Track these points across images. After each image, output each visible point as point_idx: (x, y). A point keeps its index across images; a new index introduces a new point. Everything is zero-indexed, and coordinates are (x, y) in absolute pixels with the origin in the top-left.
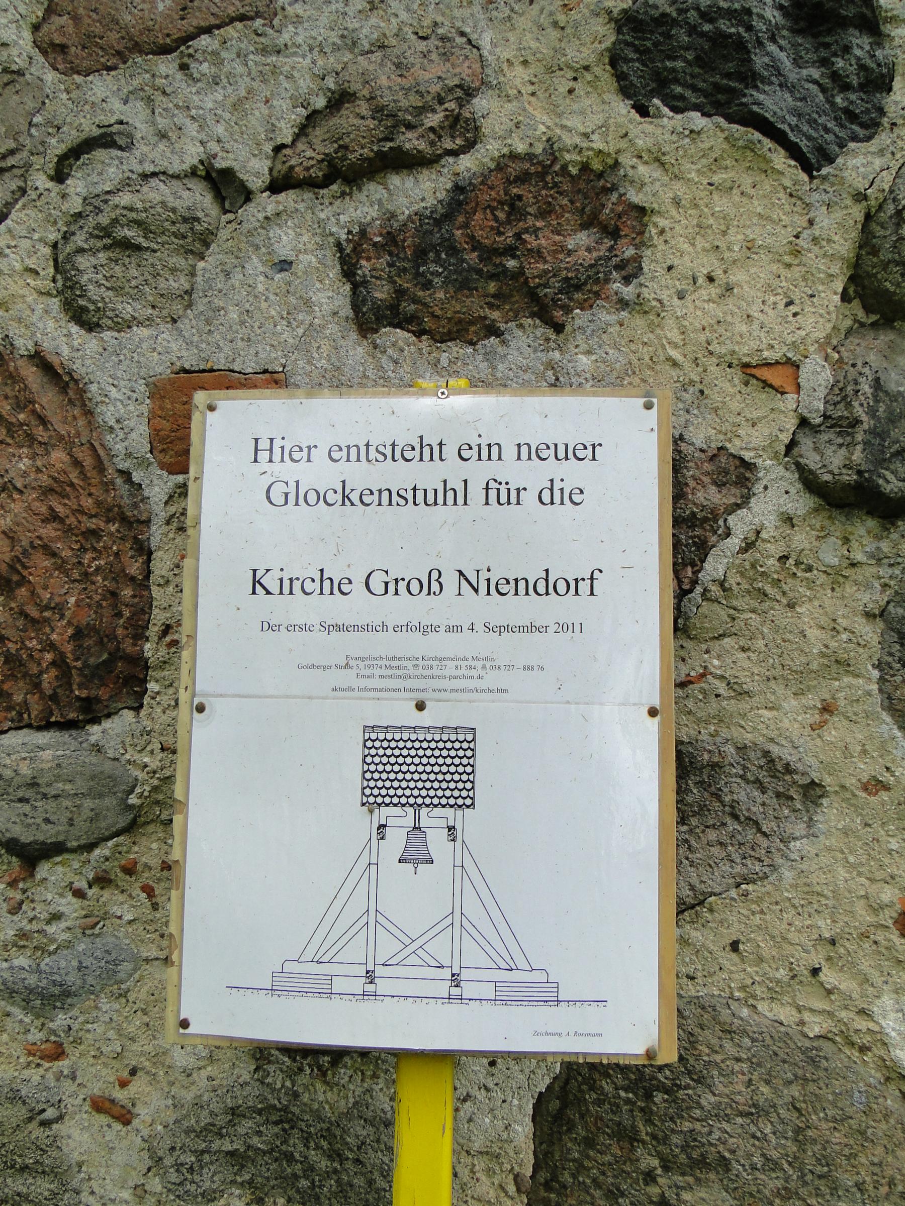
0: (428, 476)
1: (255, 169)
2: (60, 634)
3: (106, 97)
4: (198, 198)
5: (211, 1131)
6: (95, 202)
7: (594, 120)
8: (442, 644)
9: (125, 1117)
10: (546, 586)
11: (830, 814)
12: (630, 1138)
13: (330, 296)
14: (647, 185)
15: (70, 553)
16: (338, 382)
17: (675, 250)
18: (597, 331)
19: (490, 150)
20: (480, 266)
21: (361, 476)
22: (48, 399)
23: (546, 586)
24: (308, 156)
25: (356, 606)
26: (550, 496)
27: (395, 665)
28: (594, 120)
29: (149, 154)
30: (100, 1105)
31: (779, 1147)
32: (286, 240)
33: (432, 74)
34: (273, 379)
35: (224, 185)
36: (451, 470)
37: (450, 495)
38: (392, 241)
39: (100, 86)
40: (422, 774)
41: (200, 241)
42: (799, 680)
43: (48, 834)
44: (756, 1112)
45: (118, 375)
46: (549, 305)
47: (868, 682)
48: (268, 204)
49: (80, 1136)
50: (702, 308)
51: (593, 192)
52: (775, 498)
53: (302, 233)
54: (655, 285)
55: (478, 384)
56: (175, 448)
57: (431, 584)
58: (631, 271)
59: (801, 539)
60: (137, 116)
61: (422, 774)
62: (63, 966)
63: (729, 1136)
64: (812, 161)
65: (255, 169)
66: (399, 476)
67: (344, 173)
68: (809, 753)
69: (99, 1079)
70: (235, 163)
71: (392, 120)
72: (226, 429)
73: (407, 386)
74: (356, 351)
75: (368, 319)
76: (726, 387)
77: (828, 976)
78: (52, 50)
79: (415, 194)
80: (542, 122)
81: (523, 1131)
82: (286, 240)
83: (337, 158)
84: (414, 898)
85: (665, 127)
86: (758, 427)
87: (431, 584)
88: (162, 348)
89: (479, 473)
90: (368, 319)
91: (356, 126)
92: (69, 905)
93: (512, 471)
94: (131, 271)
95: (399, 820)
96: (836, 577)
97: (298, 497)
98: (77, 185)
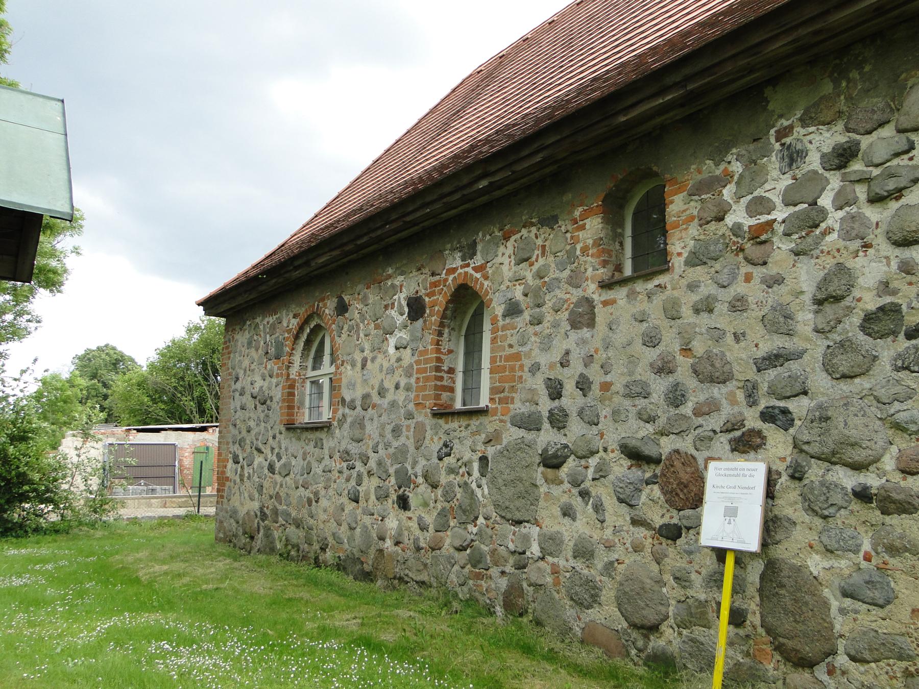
0: (735, 472)
1: (718, 430)
2: (693, 494)
3: (700, 420)
4: (711, 434)
5: (711, 576)
6: (699, 434)
7: (758, 424)
8: (735, 496)
9: (700, 574)
10: (749, 488)
11: (798, 527)
12: (771, 581)
13: (728, 447)
14: (765, 433)
15: (376, 436)
16: (728, 460)
17: (770, 442)
18: (761, 453)
19: (747, 428)
20: (746, 444)
21: (727, 472)
22: (692, 461)
23: (749, 488)
24: (725, 428)
25: (725, 490)
26: (751, 476)
27: (730, 498)
28: (758, 424)
29: (706, 428)
30: (697, 572)
31: (793, 583)
32: (722, 439)
33: (739, 418)
34: (719, 459)
35: (714, 432)
36: (739, 472)
37: (738, 475)
38: (735, 440)
39: (699, 419)
40: (731, 513)
41: (711, 439)
42: (791, 505)
43: (690, 525)
44: (789, 577)
45: (700, 457)
46: (756, 448)
47: (800, 506)
48: (720, 434)
49: (693, 576)
50: (774, 450)
51: (759, 433)
52: (784, 478)
53: (724, 438)
54: (768, 447)
55: (746, 460)
56: (706, 467)
57: (735, 487)
58: (765, 444)
59: (788, 483)
60: (704, 423)
61: (731, 513)
62: (692, 548)
63: (785, 581)
64: (786, 430)
65: (718, 430)
66: (732, 472)
67: (728, 431)
68: (794, 517)
69: (697, 567)
71: (733, 425)
72: (712, 465)
73: (735, 460)
74: (731, 455)
75: (733, 450)
76: (778, 461)
77: (800, 555)
78: (695, 414)
79: (738, 434)
80: (752, 424)
81: (758, 580)
82: (722, 439)
83: (728, 429)
84: (729, 528)
85: (767, 425)
86: (781, 467)
87: (735, 487)
88: (706, 454)
89: (742, 472)
90: (733, 450)
91: (729, 425)
92: (693, 537)
93: (746, 472)
94: (702, 443)
95: (728, 518)
96: (795, 489)
97: (719, 475)
98: (697, 432)
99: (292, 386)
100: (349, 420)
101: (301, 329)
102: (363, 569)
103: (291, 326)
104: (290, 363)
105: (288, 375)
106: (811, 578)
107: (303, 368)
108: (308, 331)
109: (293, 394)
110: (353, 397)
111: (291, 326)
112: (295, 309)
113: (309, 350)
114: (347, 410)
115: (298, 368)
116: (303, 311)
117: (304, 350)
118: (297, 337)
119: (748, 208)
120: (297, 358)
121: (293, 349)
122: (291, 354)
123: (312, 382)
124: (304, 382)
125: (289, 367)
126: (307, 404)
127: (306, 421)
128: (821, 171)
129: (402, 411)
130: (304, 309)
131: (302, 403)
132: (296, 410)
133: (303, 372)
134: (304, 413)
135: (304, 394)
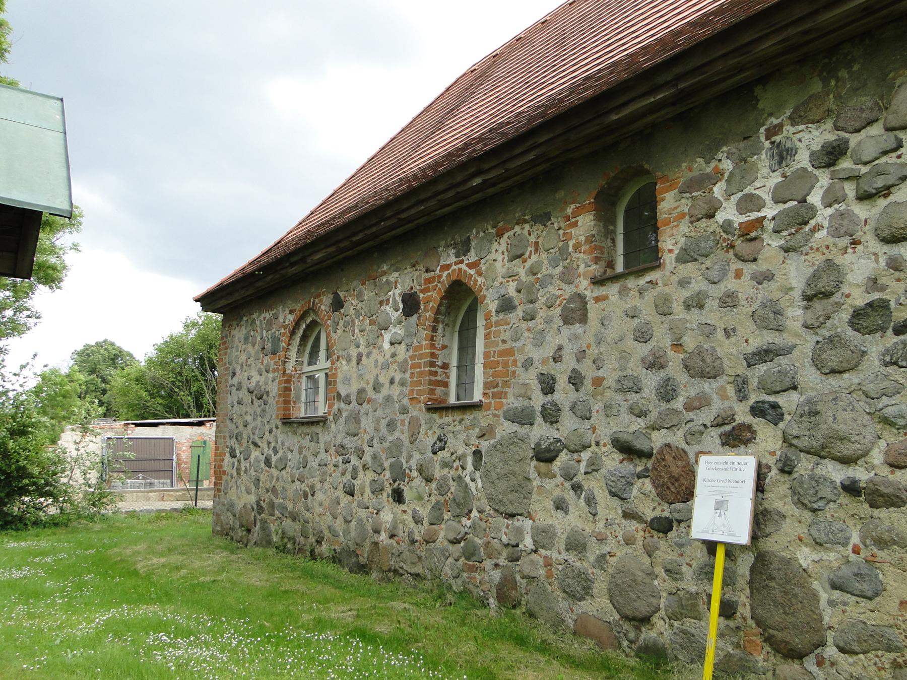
0: (726, 466)
1: (709, 424)
2: (683, 488)
3: (691, 415)
4: (702, 428)
5: (702, 568)
6: (689, 428)
7: (748, 419)
8: (725, 489)
9: (691, 566)
10: (739, 482)
11: (788, 520)
12: (761, 573)
13: (718, 441)
14: (755, 427)
16: (718, 454)
17: (760, 436)
18: (751, 447)
19: (737, 422)
20: (736, 438)
21: (718, 466)
22: (683, 455)
23: (739, 482)
24: (715, 422)
25: (716, 484)
26: (741, 470)
27: (720, 492)
28: (748, 419)
29: (696, 422)
30: (687, 564)
31: (783, 576)
32: (712, 434)
33: (729, 413)
34: (710, 453)
35: (705, 426)
36: (729, 466)
37: (728, 469)
38: (725, 434)
39: (690, 413)
40: (721, 506)
41: (702, 433)
42: (781, 498)
43: (681, 518)
44: (779, 570)
45: (691, 451)
46: (746, 442)
47: (790, 499)
48: (710, 429)
49: (684, 569)
51: (749, 428)
52: (774, 472)
53: (715, 433)
54: (758, 441)
55: (736, 454)
56: (697, 461)
57: (725, 481)
58: (755, 438)
60: (695, 417)
61: (721, 506)
62: (683, 541)
63: (775, 573)
64: (776, 424)
65: (709, 424)
66: (722, 466)
67: (719, 425)
68: (783, 510)
69: (688, 560)
70: (441, 421)
71: (724, 419)
72: (703, 459)
73: (726, 454)
74: (721, 449)
75: (723, 444)
76: (767, 455)
77: (790, 548)
78: (685, 409)
79: (728, 428)
80: (743, 419)
81: (748, 573)
82: (712, 434)
83: (719, 423)
84: (719, 521)
85: (757, 419)
86: (771, 461)
87: (725, 481)
88: (697, 448)
89: (732, 466)
90: (723, 444)
91: (720, 420)
92: (684, 530)
93: (736, 466)
94: (693, 437)
95: (718, 512)
96: (784, 482)
98: (687, 426)
99: (288, 381)
100: (344, 414)
101: (297, 324)
102: (358, 562)
103: (287, 322)
104: (286, 358)
105: (285, 370)
106: (801, 570)
107: (299, 363)
108: (304, 326)
109: (289, 389)
110: (348, 391)
111: (287, 322)
112: (291, 305)
113: (305, 346)
114: (342, 405)
115: (294, 363)
116: (299, 307)
117: (300, 345)
118: (293, 333)
119: (738, 205)
120: (293, 354)
121: (289, 344)
122: (287, 350)
123: (308, 377)
124: (300, 377)
125: (285, 362)
126: (303, 399)
127: (302, 415)
128: (810, 169)
129: (397, 406)
130: (300, 305)
131: (298, 398)
132: (292, 405)
133: (299, 367)
134: (300, 408)
135: (300, 389)
